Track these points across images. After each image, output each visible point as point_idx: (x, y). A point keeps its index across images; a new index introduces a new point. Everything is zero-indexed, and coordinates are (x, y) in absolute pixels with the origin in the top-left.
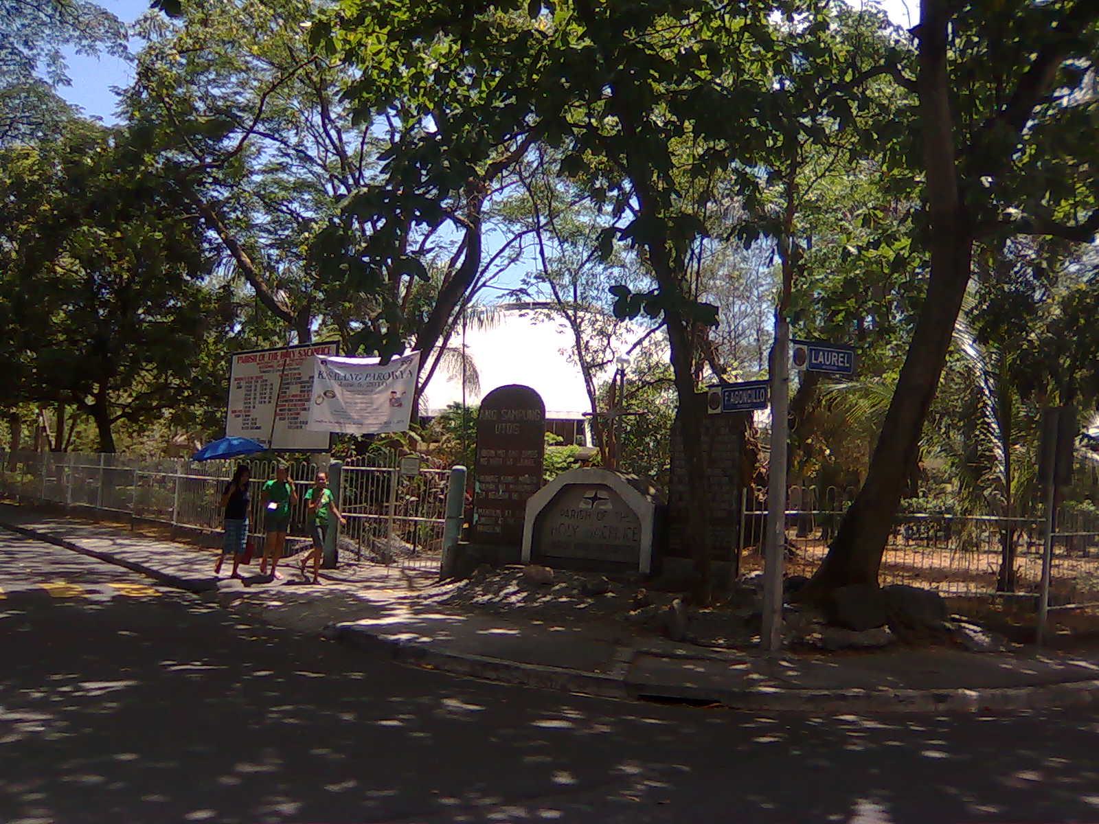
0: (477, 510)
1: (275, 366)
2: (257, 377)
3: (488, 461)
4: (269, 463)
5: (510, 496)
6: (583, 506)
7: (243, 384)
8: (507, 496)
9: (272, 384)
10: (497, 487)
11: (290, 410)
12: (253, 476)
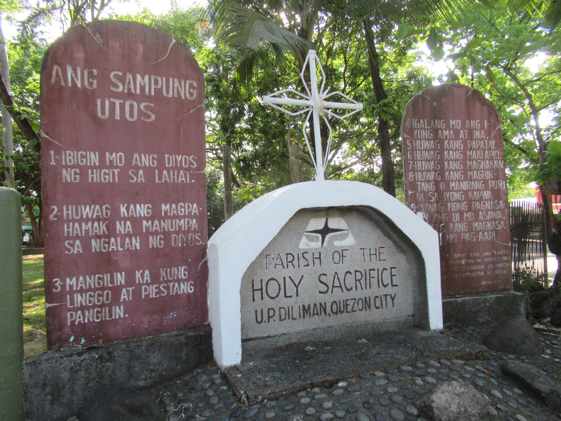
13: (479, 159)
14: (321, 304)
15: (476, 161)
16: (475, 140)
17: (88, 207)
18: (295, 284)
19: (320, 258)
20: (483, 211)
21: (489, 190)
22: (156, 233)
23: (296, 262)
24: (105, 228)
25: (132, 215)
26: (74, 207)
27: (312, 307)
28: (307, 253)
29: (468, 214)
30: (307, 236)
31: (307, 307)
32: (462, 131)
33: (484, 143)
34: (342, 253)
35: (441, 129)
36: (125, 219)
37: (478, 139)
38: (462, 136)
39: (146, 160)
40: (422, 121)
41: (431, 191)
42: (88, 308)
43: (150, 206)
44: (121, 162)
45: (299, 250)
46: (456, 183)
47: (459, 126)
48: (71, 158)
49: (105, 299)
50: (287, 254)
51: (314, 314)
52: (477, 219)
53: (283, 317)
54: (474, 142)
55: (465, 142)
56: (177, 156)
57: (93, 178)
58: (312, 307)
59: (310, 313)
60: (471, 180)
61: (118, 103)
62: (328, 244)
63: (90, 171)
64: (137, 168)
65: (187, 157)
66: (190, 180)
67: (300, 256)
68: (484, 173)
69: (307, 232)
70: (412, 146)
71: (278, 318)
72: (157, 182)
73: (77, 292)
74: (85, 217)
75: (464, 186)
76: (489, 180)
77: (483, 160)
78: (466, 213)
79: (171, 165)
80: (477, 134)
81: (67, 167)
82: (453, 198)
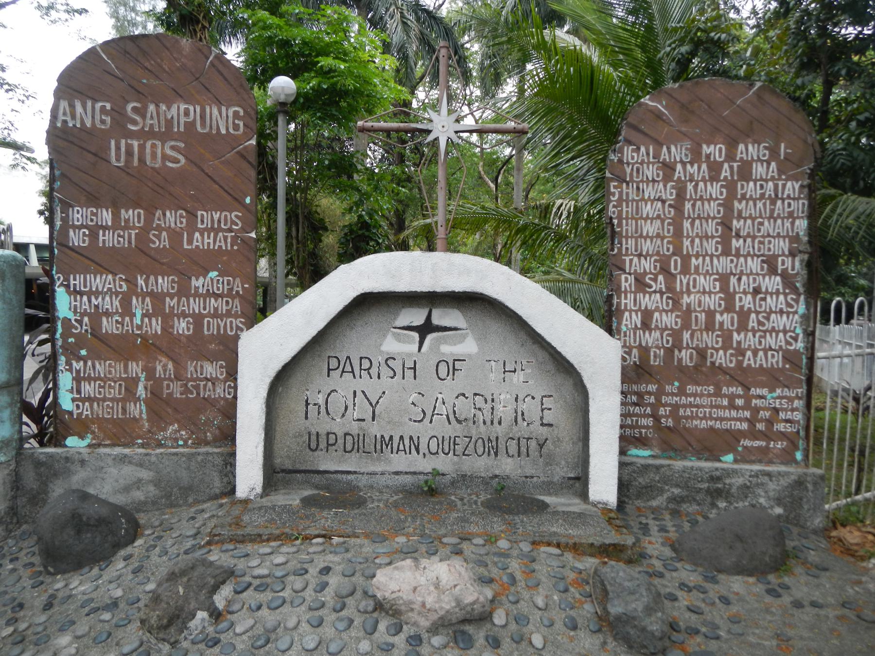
0: (69, 363)
13: (761, 217)
14: (411, 438)
15: (753, 219)
16: (755, 181)
17: (98, 277)
18: (371, 404)
19: (414, 368)
20: (758, 313)
21: (776, 274)
22: (184, 315)
23: (374, 371)
24: (118, 303)
25: (152, 290)
26: (82, 276)
27: (396, 440)
28: (394, 359)
29: (725, 315)
30: (394, 334)
31: (387, 439)
32: (726, 166)
33: (776, 187)
34: (453, 366)
35: (681, 161)
36: (144, 295)
37: (761, 179)
38: (725, 172)
39: (172, 218)
40: (643, 149)
41: (651, 273)
42: (98, 400)
43: (176, 280)
44: (139, 222)
45: (382, 352)
46: (704, 260)
47: (720, 156)
48: (79, 216)
49: (117, 392)
50: (361, 358)
51: (398, 450)
52: (743, 327)
53: (349, 448)
54: (751, 184)
55: (731, 187)
56: (214, 213)
57: (104, 241)
58: (396, 440)
59: (392, 448)
60: (738, 255)
61: (135, 144)
62: (430, 348)
63: (101, 232)
64: (159, 228)
65: (228, 214)
66: (232, 246)
67: (383, 362)
68: (770, 242)
69: (395, 328)
70: (621, 193)
71: (342, 447)
72: (186, 246)
73: (84, 379)
74: (94, 289)
75: (723, 264)
76: (779, 256)
77: (769, 219)
78: (722, 314)
79: (205, 226)
80: (759, 170)
81: (75, 227)
82: (694, 287)
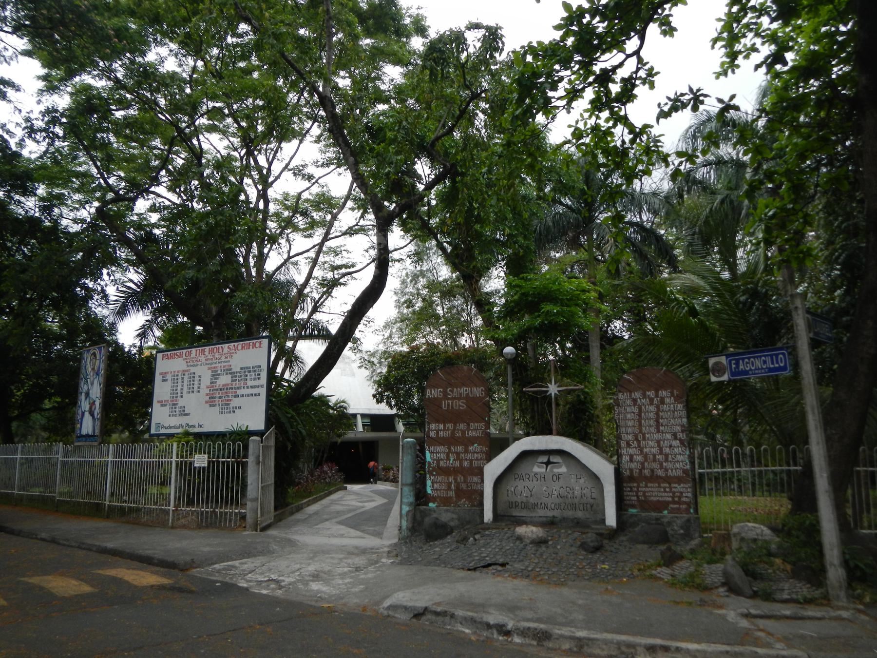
1: (203, 360)
2: (184, 371)
3: (437, 433)
4: (214, 444)
5: (461, 464)
6: (536, 469)
7: (169, 377)
8: (457, 464)
9: (200, 377)
10: (448, 456)
11: (220, 397)
12: (866, 524)
